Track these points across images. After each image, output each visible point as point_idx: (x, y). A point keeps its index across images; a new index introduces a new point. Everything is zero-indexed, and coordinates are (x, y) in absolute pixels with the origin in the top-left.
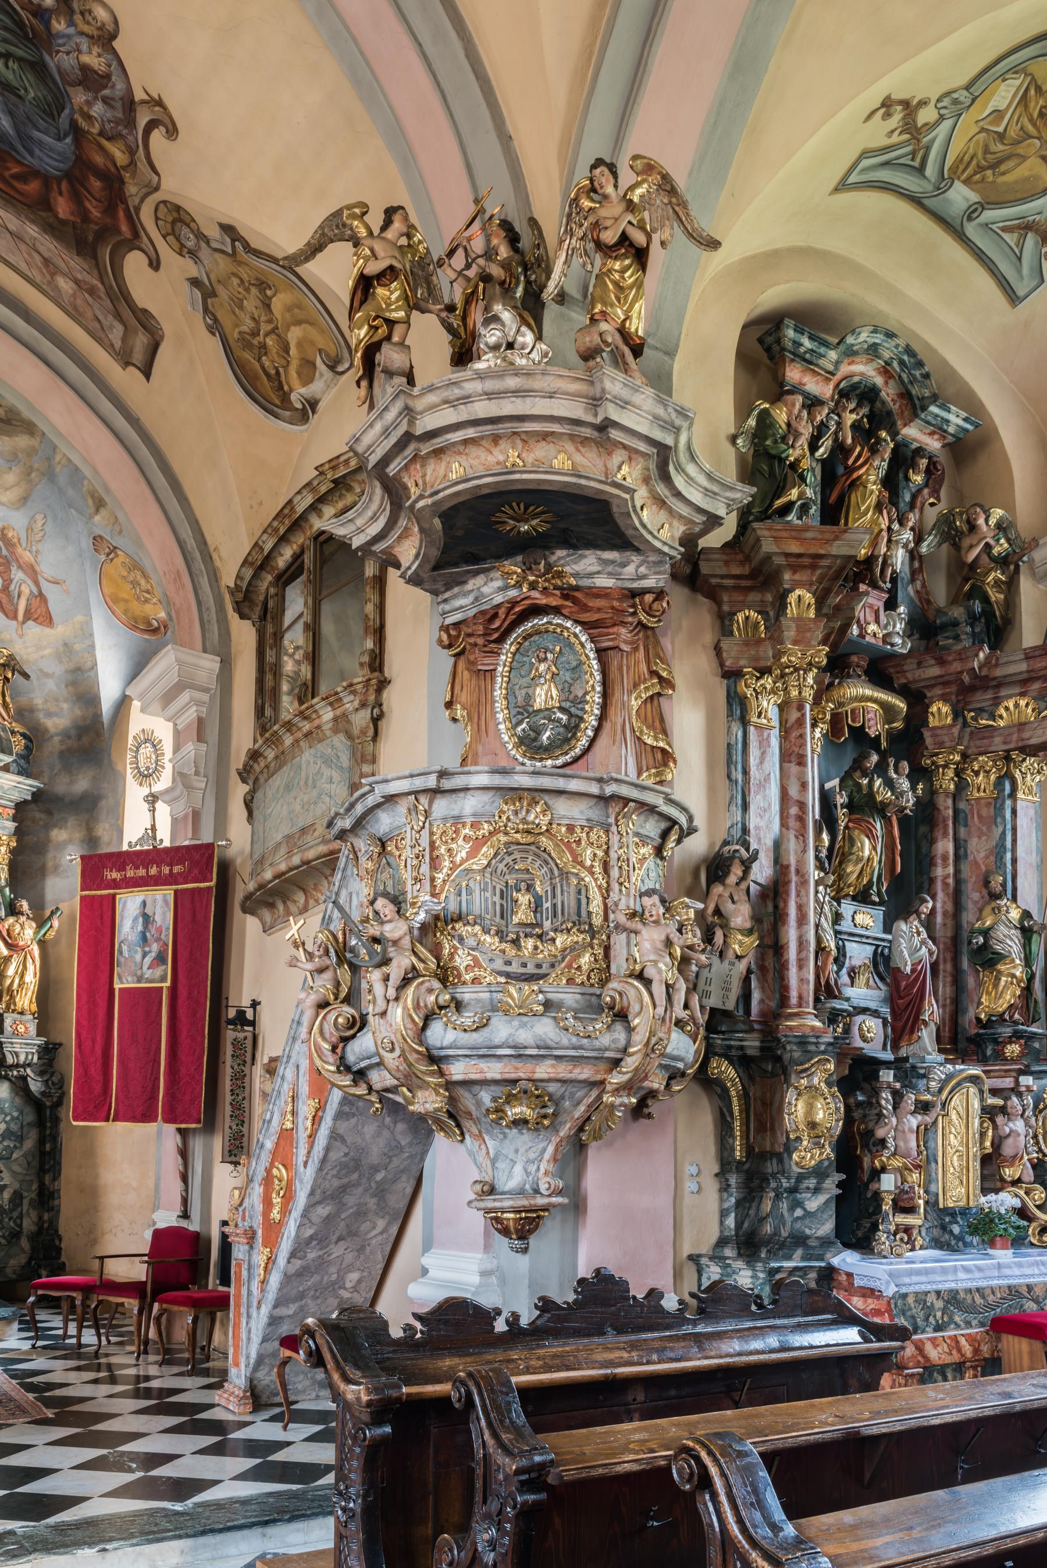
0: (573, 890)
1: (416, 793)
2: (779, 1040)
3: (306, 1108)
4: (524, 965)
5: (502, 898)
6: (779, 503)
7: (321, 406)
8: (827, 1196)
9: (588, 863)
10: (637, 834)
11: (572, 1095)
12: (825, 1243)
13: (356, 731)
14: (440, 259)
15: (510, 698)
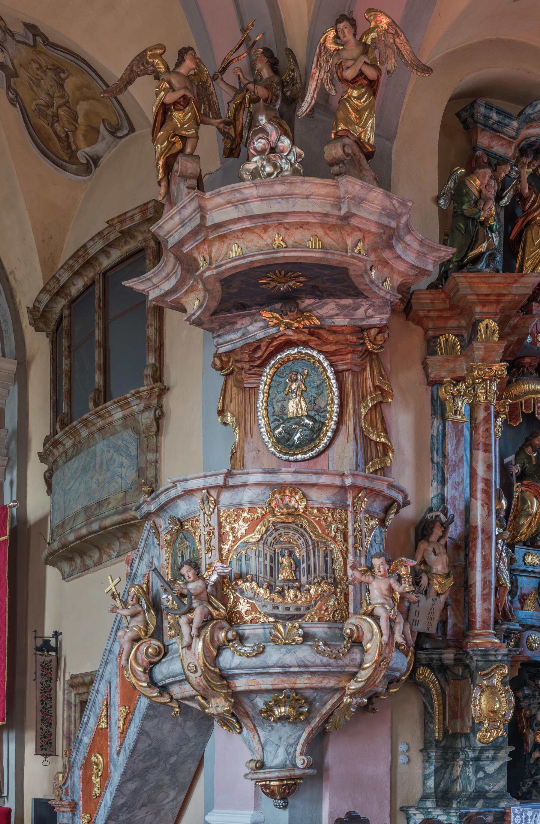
0: (322, 553)
1: (208, 489)
2: (468, 653)
3: (118, 713)
4: (288, 609)
5: (271, 561)
6: (473, 254)
7: (103, 162)
8: (502, 763)
9: (333, 534)
10: (367, 511)
11: (321, 698)
12: (499, 796)
13: (142, 428)
14: (214, 75)
15: (270, 408)
